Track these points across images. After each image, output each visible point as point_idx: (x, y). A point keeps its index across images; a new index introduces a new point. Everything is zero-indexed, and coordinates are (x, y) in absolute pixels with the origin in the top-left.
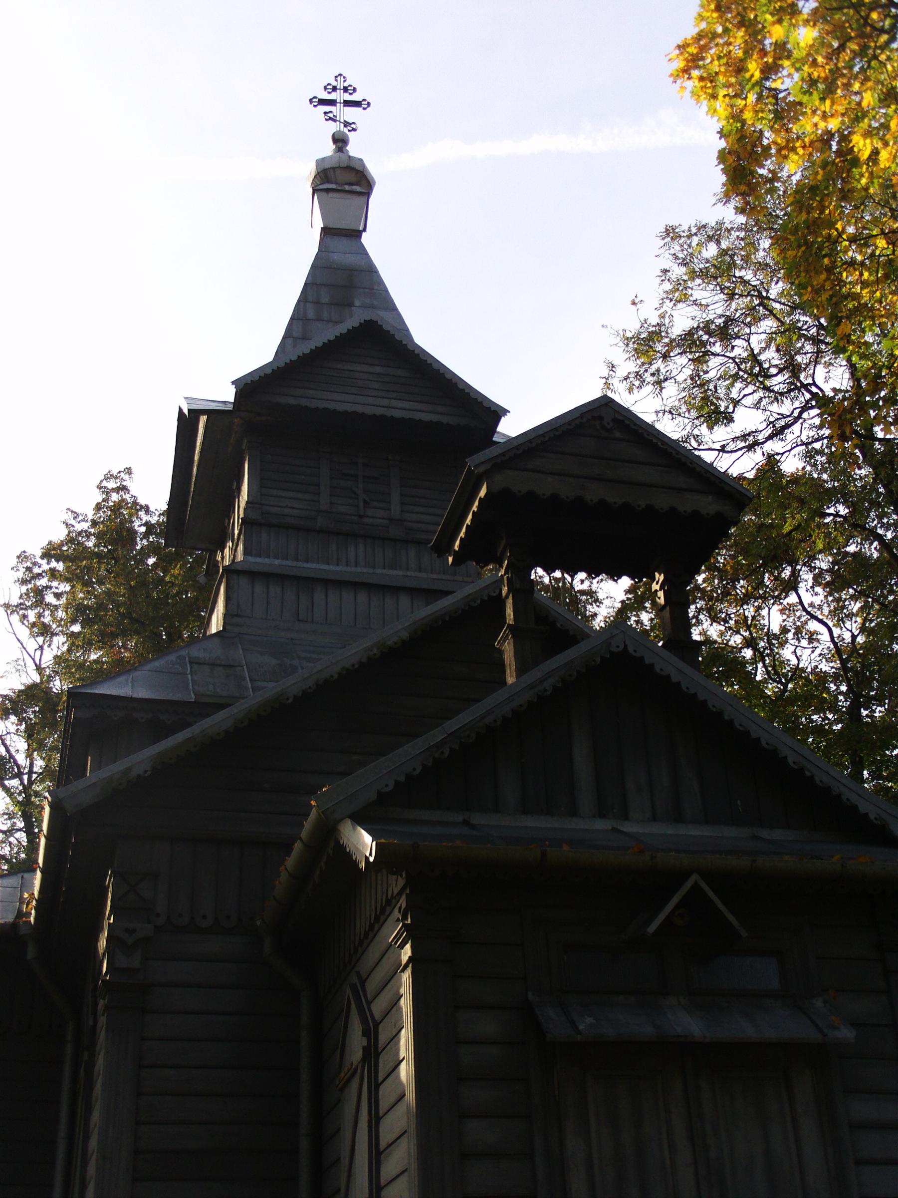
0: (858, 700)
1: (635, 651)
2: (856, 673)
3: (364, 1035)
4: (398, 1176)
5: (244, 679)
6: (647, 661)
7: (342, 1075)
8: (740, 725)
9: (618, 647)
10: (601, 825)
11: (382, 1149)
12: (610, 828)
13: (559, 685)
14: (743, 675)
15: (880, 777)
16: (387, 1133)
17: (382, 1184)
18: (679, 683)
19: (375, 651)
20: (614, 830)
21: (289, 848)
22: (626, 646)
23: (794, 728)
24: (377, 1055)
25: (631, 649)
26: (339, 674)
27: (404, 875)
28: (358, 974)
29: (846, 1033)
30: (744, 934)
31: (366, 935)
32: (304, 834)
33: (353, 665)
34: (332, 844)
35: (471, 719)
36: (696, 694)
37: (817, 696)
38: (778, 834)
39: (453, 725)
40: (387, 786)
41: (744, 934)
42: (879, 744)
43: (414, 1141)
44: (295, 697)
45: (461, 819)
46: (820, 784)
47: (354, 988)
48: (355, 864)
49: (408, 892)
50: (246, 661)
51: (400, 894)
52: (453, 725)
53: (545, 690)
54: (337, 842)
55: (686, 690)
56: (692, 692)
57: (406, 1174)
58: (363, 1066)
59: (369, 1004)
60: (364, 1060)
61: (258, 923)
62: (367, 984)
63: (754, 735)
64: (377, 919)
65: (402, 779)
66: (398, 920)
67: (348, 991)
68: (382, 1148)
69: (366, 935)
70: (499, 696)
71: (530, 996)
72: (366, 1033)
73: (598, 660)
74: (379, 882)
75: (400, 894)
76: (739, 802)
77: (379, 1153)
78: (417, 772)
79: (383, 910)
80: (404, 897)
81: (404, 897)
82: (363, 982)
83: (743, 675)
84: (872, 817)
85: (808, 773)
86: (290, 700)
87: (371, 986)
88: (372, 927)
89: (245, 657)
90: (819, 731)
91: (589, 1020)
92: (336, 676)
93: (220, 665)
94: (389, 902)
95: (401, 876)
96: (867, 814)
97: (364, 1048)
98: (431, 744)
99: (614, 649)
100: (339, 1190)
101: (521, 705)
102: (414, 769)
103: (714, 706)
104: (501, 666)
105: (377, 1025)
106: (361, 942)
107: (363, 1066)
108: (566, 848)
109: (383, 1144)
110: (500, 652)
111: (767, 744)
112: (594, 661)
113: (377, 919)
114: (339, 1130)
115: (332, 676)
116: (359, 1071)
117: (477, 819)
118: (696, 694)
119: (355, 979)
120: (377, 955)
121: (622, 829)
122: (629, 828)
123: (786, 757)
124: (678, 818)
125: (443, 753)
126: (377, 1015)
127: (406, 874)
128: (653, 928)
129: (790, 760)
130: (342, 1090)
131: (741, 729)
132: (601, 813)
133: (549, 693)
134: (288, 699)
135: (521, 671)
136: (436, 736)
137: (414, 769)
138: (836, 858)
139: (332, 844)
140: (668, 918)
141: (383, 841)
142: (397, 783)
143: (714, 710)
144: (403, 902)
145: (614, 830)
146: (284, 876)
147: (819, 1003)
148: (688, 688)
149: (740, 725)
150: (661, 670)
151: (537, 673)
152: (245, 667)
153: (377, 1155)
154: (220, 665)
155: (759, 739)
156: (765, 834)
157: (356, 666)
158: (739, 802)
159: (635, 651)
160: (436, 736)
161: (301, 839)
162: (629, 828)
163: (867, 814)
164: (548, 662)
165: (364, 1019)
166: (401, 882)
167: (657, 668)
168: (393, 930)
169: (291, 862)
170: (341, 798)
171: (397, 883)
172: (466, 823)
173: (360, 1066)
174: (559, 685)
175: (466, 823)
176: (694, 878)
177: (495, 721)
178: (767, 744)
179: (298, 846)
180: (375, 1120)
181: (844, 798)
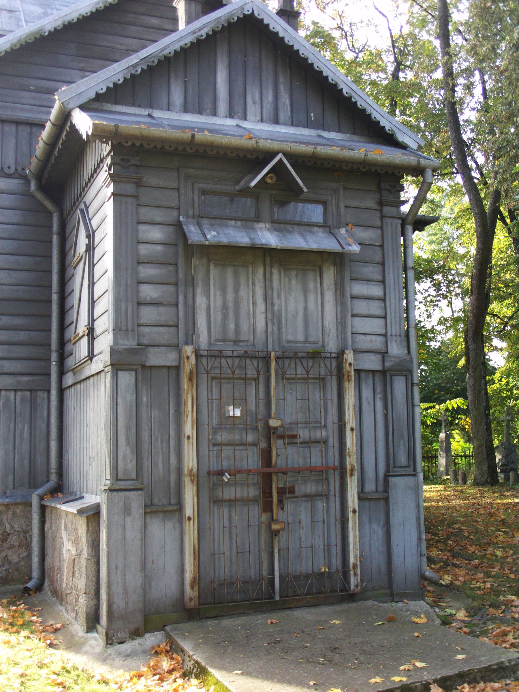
0: (399, 66)
1: (259, 15)
2: (400, 51)
3: (87, 237)
4: (103, 314)
5: (21, 20)
6: (266, 22)
7: (75, 260)
8: (318, 67)
9: (248, 11)
10: (231, 122)
11: (95, 300)
12: (235, 124)
13: (211, 33)
14: (333, 45)
15: (405, 114)
16: (98, 290)
17: (95, 318)
18: (283, 38)
19: (101, 5)
20: (238, 126)
21: (43, 127)
22: (253, 11)
23: (358, 80)
24: (94, 249)
25: (256, 14)
26: (78, 19)
27: (110, 144)
28: (85, 203)
29: (355, 248)
30: (305, 190)
31: (89, 180)
32: (52, 117)
33: (87, 13)
34: (69, 124)
35: (155, 51)
36: (293, 45)
37: (376, 63)
38: (333, 135)
39: (144, 53)
40: (102, 89)
41: (305, 190)
42: (407, 94)
43: (111, 295)
44: (50, 32)
45: (147, 113)
46: (360, 107)
47: (82, 211)
48: (80, 136)
49: (112, 154)
50: (22, 8)
51: (108, 155)
52: (144, 53)
53: (202, 36)
54: (71, 123)
55: (287, 42)
56: (291, 44)
57: (107, 313)
58: (86, 255)
59: (90, 220)
60: (86, 251)
61: (27, 172)
62: (89, 209)
63: (325, 74)
64: (95, 171)
65: (111, 85)
66: (106, 171)
67: (78, 212)
68: (95, 299)
69: (89, 180)
70: (173, 37)
71: (181, 219)
72: (88, 236)
73: (236, 19)
74: (97, 149)
75: (108, 155)
76: (312, 115)
77: (94, 302)
78: (120, 82)
79: (99, 165)
80: (110, 157)
81: (110, 157)
82: (87, 208)
83: (333, 45)
84: (387, 129)
85: (354, 100)
86: (47, 34)
87: (91, 210)
88: (92, 175)
89: (22, 5)
90: (373, 83)
91: (214, 233)
92: (75, 20)
93: (5, 10)
94: (102, 161)
95: (108, 144)
96: (385, 127)
97: (87, 245)
98: (130, 65)
99: (246, 13)
100: (73, 322)
101: (186, 44)
102: (119, 80)
103: (303, 54)
104: (175, 20)
105: (94, 232)
106: (86, 185)
107: (86, 255)
108: (206, 133)
109: (96, 297)
110: (175, 9)
111: (332, 80)
112: (233, 19)
113: (95, 171)
114: (73, 290)
115: (73, 20)
116: (84, 257)
117: (156, 113)
118: (293, 45)
119: (82, 206)
120: (95, 192)
121: (242, 125)
122: (246, 125)
123: (342, 89)
124: (276, 121)
125: (137, 71)
126: (95, 228)
127: (112, 143)
128: (253, 184)
129: (344, 92)
130: (75, 268)
131: (318, 69)
132: (231, 115)
133: (204, 37)
134: (45, 33)
135: (189, 22)
136: (134, 59)
137: (119, 80)
138: (363, 150)
139: (69, 124)
140: (263, 178)
141: (97, 122)
142: (108, 88)
143: (303, 56)
144: (109, 160)
145: (238, 126)
146: (41, 144)
147: (343, 231)
148: (288, 41)
149: (318, 67)
150: (274, 28)
151: (197, 24)
152: (22, 13)
153: (92, 303)
154: (5, 10)
155: (327, 77)
156: (325, 134)
157: (89, 14)
158: (312, 115)
159: (259, 15)
160: (134, 59)
161: (50, 120)
162: (246, 125)
163: (385, 127)
164: (205, 17)
165: (87, 229)
166: (109, 148)
167: (271, 27)
168: (103, 175)
169: (45, 134)
170: (73, 95)
171: (106, 148)
172: (150, 116)
173: (84, 254)
174: (211, 33)
175: (150, 116)
176: (280, 156)
177: (170, 53)
178: (332, 80)
179: (48, 125)
180: (92, 284)
181: (373, 116)
